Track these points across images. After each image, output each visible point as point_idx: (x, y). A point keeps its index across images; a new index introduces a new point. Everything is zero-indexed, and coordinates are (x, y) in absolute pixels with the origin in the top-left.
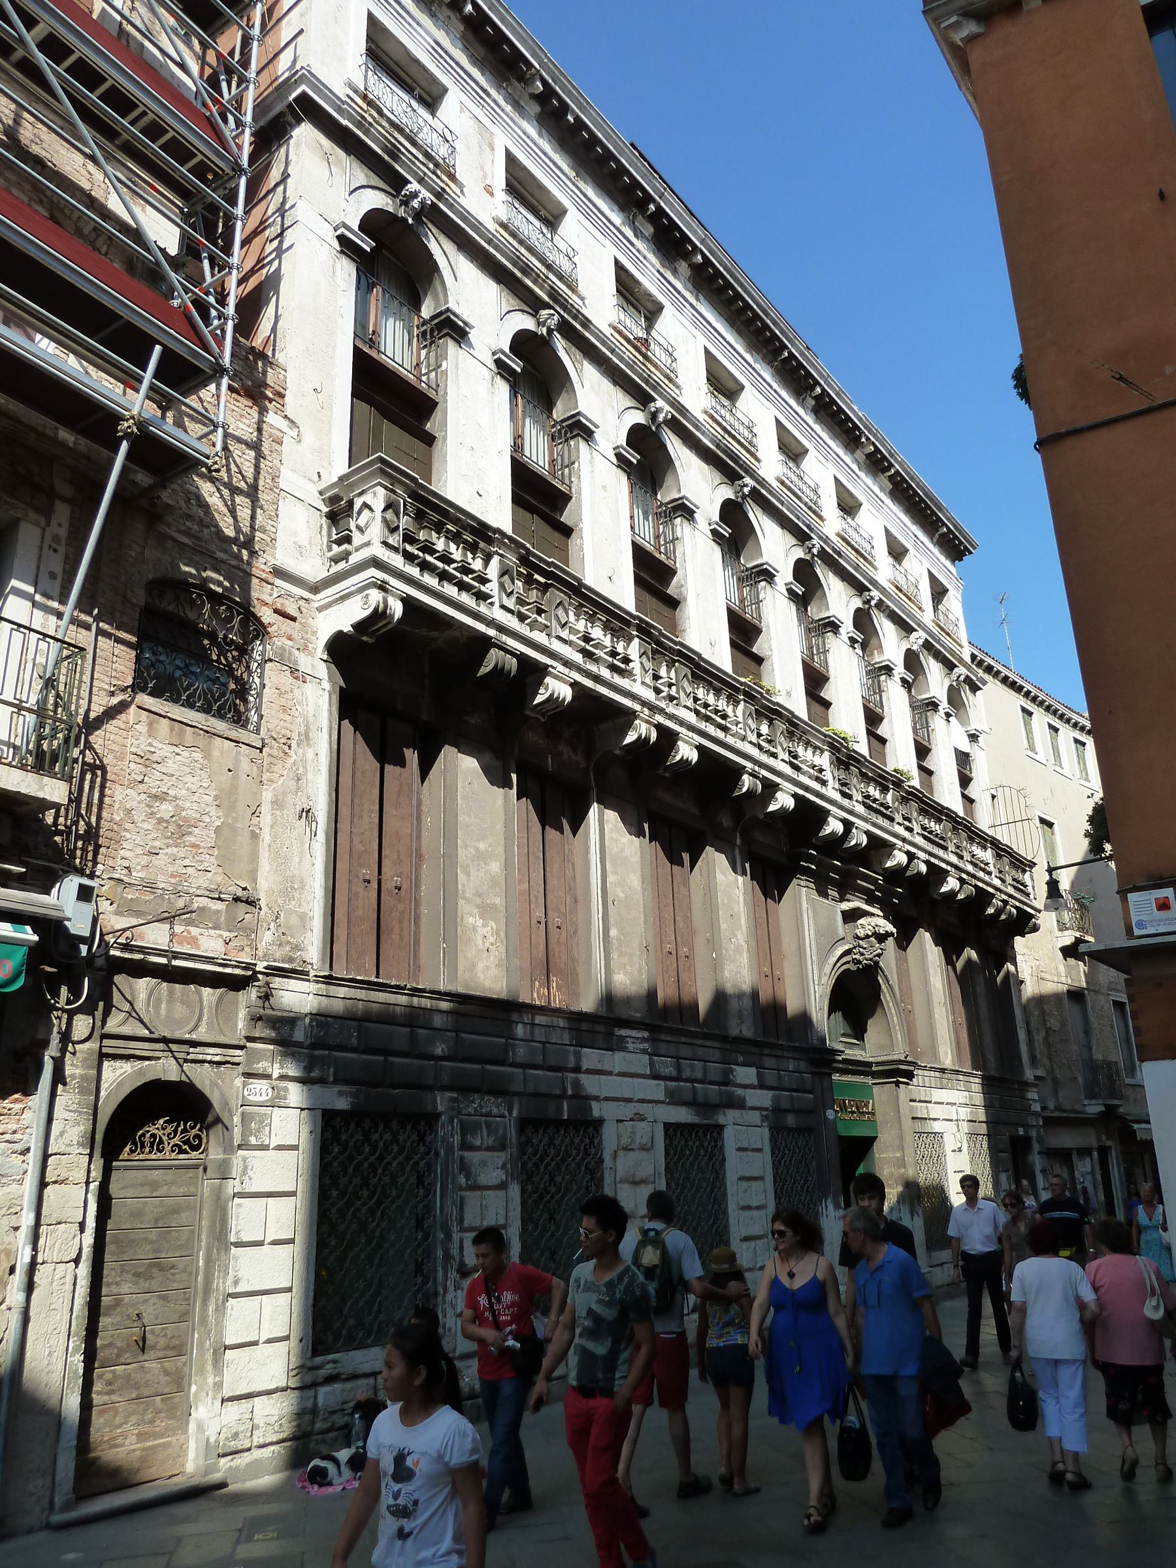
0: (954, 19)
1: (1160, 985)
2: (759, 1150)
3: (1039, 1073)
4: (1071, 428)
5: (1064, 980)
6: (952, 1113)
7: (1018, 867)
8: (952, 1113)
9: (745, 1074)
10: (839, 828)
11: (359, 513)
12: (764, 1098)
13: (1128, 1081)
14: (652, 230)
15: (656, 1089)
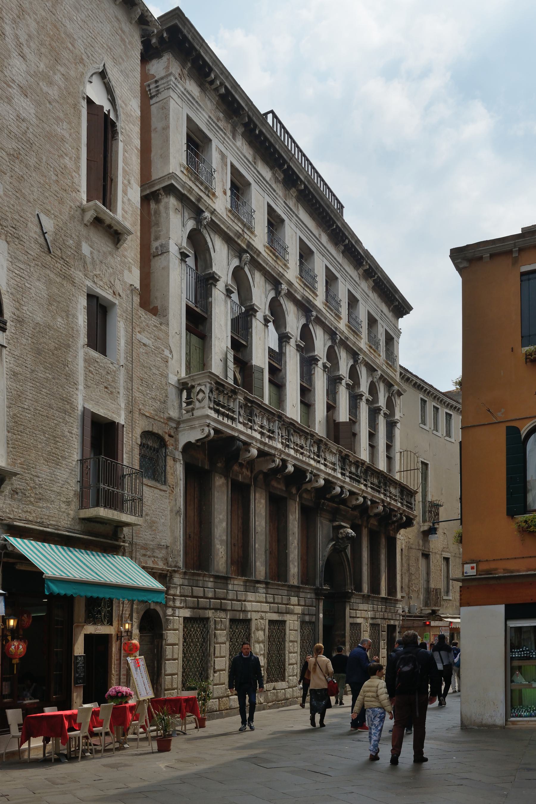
0: (459, 260)
1: (468, 588)
2: (296, 630)
3: (404, 594)
4: (472, 425)
5: (421, 548)
6: (364, 614)
8: (364, 614)
9: (294, 600)
10: (338, 489)
11: (198, 393)
13: (445, 598)
14: (282, 176)
15: (266, 607)
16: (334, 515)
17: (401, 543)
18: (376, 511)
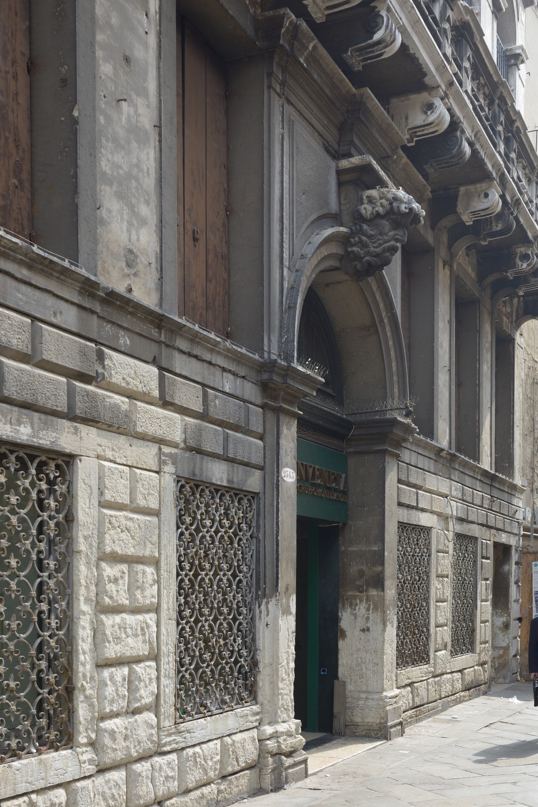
6: (439, 504)
8: (439, 504)
9: (129, 370)
12: (173, 426)
18: (480, 205)
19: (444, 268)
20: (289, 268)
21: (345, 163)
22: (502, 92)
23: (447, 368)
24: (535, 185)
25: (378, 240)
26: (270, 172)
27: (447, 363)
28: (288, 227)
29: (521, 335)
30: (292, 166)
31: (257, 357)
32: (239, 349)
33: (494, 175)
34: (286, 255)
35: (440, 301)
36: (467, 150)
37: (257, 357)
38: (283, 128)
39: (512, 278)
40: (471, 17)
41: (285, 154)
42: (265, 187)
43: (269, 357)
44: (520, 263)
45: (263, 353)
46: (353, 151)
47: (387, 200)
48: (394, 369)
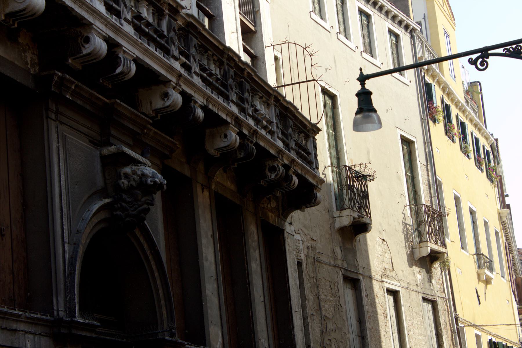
5: (339, 263)
7: (301, 132)
16: (103, 124)
17: (297, 247)
18: (222, 143)
19: (203, 192)
20: (69, 243)
21: (106, 151)
22: (228, 55)
23: (215, 277)
24: (273, 107)
25: (135, 205)
26: (51, 177)
27: (214, 274)
28: (66, 213)
29: (291, 224)
30: (66, 168)
31: (49, 317)
32: (35, 316)
33: (229, 120)
34: (66, 235)
35: (202, 221)
36: (200, 113)
37: (49, 317)
38: (58, 143)
39: (266, 186)
40: (192, 19)
41: (61, 161)
42: (48, 189)
43: (58, 314)
44: (269, 174)
45: (53, 312)
46: (112, 140)
47: (138, 175)
48: (161, 294)
